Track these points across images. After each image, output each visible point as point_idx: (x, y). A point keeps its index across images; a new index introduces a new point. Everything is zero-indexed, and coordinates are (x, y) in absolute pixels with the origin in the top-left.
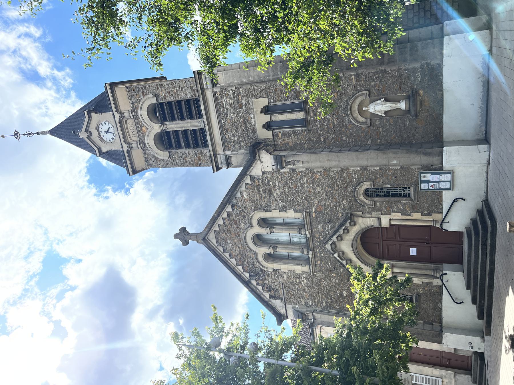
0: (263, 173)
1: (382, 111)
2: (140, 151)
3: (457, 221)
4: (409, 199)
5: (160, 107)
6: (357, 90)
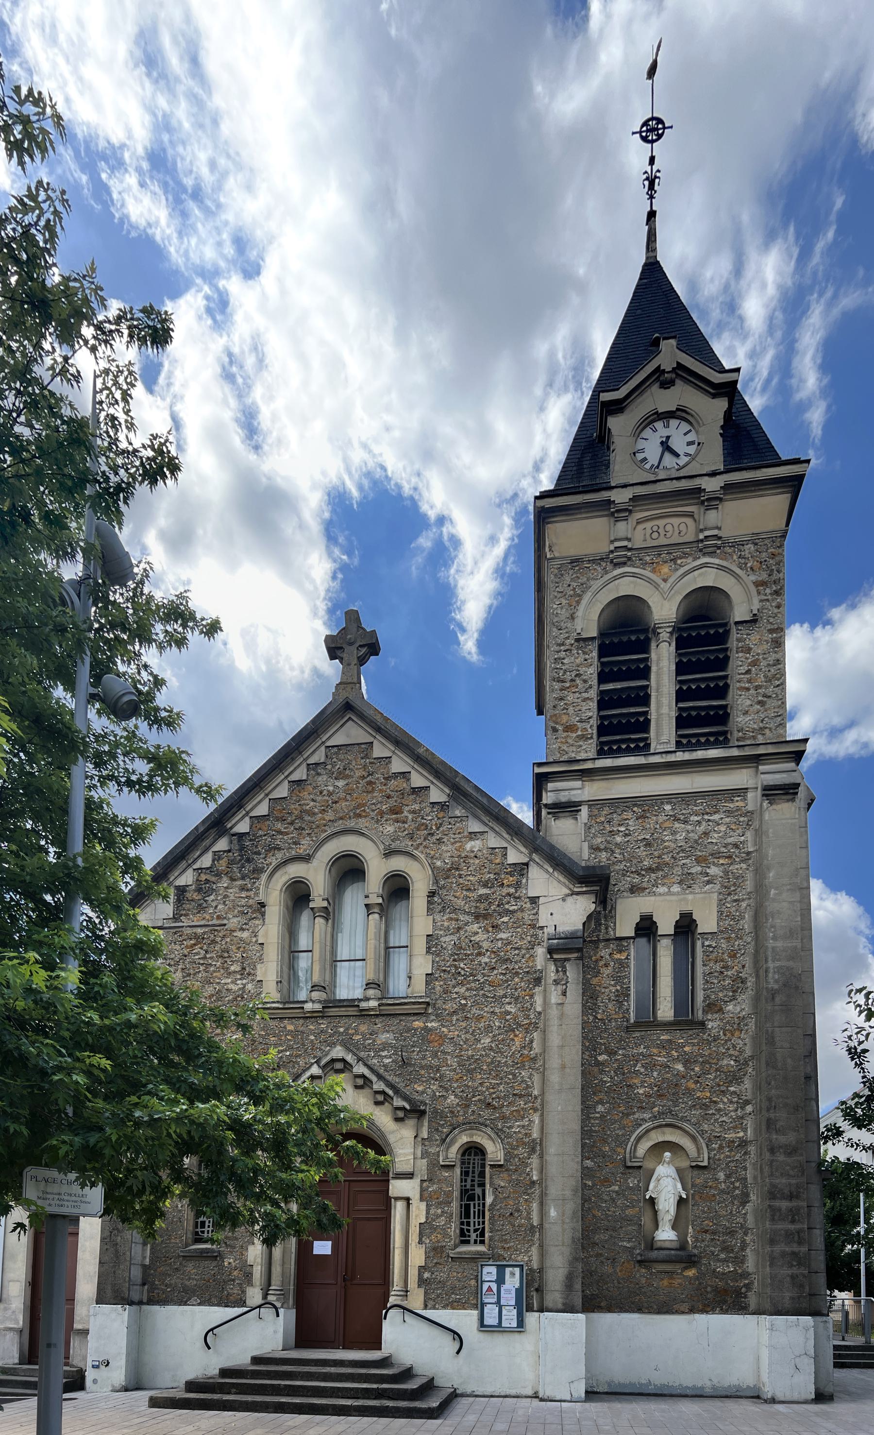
0: (534, 900)
1: (659, 1192)
2: (604, 547)
3: (405, 1339)
4: (457, 1241)
5: (629, 668)
6: (710, 1140)
